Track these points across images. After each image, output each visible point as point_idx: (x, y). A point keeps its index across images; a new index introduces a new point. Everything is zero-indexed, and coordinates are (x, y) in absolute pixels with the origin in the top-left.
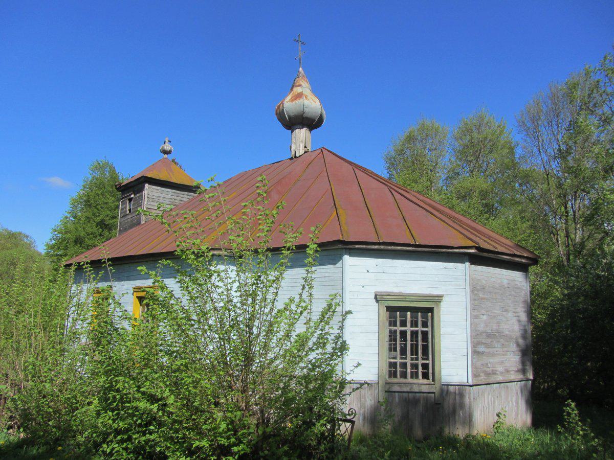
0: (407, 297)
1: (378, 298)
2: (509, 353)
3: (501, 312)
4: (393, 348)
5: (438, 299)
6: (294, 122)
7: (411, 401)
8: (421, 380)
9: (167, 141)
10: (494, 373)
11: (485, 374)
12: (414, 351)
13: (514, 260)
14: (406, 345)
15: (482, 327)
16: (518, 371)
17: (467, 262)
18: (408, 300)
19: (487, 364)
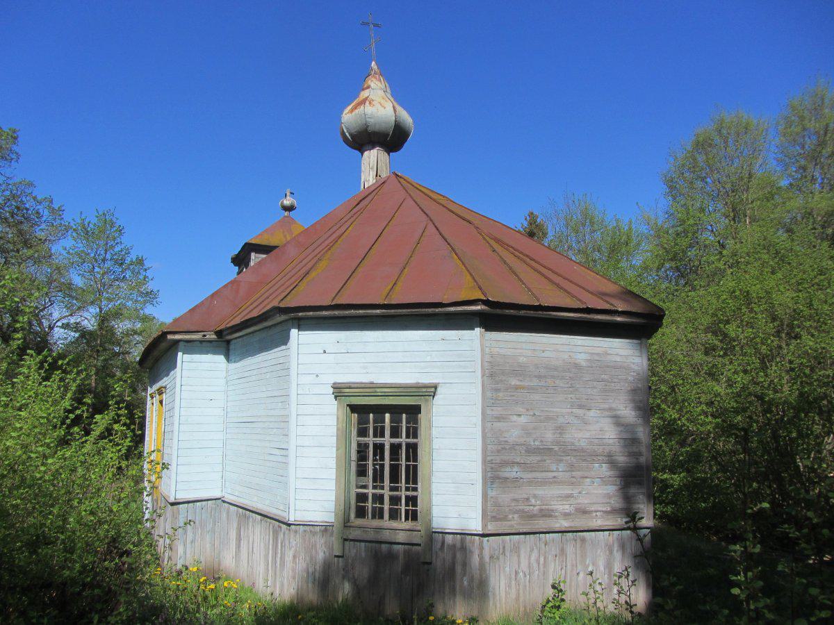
0: (378, 390)
1: (339, 391)
2: (588, 480)
3: (570, 410)
4: (362, 472)
5: (430, 391)
6: (363, 139)
7: (381, 554)
8: (403, 524)
9: (288, 194)
10: (547, 514)
11: (521, 517)
12: (395, 477)
13: (556, 316)
14: (382, 466)
15: (514, 435)
16: (614, 511)
17: (477, 327)
18: (380, 394)
19: (528, 499)
